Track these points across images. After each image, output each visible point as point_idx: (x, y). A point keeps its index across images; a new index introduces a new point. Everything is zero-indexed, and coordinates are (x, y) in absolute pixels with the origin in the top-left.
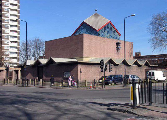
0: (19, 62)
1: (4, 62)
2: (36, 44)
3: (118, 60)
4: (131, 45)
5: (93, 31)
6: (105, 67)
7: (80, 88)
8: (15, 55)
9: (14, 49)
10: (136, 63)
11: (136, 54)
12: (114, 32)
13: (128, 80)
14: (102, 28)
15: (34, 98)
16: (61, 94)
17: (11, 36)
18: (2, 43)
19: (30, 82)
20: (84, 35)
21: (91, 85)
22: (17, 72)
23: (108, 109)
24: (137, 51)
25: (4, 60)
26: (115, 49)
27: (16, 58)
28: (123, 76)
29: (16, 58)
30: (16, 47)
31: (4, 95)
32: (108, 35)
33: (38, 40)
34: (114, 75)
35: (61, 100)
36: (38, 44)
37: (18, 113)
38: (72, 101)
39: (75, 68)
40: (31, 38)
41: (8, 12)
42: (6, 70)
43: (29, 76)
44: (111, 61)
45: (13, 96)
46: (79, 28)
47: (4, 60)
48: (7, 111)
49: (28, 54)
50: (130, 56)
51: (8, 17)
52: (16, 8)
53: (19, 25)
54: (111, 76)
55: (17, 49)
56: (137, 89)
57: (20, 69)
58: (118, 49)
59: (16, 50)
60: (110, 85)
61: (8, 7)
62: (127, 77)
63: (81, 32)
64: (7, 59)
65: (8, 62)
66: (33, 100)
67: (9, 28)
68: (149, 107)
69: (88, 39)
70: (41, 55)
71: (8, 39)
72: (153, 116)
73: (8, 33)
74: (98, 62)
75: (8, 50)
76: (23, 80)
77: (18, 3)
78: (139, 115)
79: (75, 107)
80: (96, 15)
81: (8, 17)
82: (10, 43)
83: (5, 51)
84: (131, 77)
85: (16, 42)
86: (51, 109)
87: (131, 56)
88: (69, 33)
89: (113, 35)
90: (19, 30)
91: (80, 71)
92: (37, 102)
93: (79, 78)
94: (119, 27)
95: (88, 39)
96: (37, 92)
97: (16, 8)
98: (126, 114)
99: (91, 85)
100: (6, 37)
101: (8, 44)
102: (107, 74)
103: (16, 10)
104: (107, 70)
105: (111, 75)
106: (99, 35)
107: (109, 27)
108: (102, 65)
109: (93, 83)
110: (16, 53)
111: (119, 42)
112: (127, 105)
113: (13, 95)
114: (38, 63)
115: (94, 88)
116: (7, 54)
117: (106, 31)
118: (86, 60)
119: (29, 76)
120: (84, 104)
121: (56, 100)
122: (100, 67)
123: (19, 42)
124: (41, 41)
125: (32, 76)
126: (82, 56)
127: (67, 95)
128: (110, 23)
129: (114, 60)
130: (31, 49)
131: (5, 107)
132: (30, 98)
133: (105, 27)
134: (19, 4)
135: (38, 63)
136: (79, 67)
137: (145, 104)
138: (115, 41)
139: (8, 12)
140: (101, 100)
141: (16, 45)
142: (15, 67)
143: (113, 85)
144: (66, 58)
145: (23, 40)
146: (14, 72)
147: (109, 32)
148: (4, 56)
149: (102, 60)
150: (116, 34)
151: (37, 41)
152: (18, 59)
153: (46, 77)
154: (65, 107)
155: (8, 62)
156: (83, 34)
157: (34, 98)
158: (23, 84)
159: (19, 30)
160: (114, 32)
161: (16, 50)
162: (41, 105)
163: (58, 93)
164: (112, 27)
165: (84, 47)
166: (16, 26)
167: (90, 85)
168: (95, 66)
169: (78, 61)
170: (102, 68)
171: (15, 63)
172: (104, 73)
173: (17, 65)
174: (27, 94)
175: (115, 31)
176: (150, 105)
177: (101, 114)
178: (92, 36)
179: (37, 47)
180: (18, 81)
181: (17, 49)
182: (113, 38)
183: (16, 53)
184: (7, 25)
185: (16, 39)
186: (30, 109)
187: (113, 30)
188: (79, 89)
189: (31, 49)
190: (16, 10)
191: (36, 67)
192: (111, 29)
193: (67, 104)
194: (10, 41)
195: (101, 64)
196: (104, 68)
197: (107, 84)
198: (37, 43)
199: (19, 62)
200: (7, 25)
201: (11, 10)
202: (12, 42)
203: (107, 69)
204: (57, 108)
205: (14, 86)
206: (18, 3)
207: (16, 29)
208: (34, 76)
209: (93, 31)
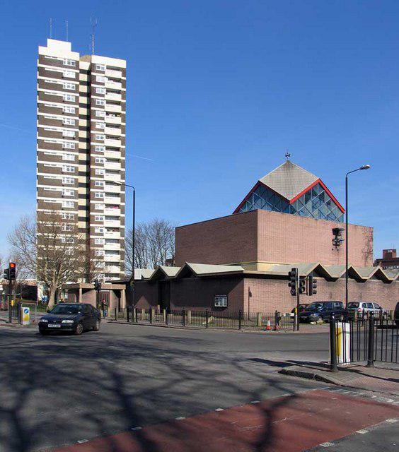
0: (122, 272)
1: (95, 271)
2: (158, 234)
3: (335, 268)
4: (368, 234)
5: (280, 203)
6: (301, 285)
7: (244, 330)
8: (116, 258)
9: (114, 244)
10: (379, 275)
11: (386, 253)
12: (328, 204)
13: (356, 313)
14: (301, 195)
15: (140, 348)
16: (199, 342)
17: (107, 217)
18: (91, 232)
19: (144, 314)
20: (260, 212)
21: (269, 324)
22: (117, 293)
23: (280, 372)
24: (389, 247)
25: (94, 269)
26: (331, 244)
27: (116, 264)
28: (344, 305)
29: (116, 264)
30: (117, 241)
31: (86, 341)
32: (316, 212)
33: (162, 225)
34: (324, 303)
35: (194, 352)
36: (162, 234)
37: (102, 374)
38: (213, 356)
39: (238, 286)
40: (146, 218)
41: (103, 165)
42: (95, 289)
43: (142, 301)
44: (319, 271)
45: (102, 342)
46: (249, 197)
47: (94, 269)
48: (82, 370)
49: (142, 254)
50: (366, 258)
51: (102, 177)
52: (117, 155)
53: (123, 192)
54: (317, 304)
55: (119, 245)
56: (348, 333)
57: (123, 287)
58: (337, 243)
59: (116, 247)
60: (312, 323)
61: (102, 153)
62: (355, 307)
63: (254, 205)
64: (99, 267)
65: (102, 272)
66: (137, 351)
67: (103, 200)
68: (366, 371)
69: (269, 223)
70: (169, 257)
71: (102, 223)
72: (361, 386)
73: (102, 211)
74: (285, 271)
75: (102, 246)
76: (128, 310)
77: (122, 145)
78: (337, 385)
79: (214, 367)
80: (288, 166)
81: (102, 177)
82: (105, 230)
83: (97, 248)
84: (364, 306)
85: (118, 228)
86: (166, 368)
87: (369, 260)
88: (226, 209)
89: (326, 210)
90: (123, 204)
91: (247, 292)
92: (143, 356)
93: (246, 310)
94: (337, 192)
95: (269, 223)
96: (150, 337)
97: (117, 155)
98: (314, 381)
99: (269, 324)
100: (97, 218)
101: (102, 235)
102: (306, 300)
103: (118, 160)
104: (305, 292)
105: (316, 303)
106: (293, 211)
107: (317, 194)
108: (294, 281)
109: (274, 320)
110: (117, 252)
111: (339, 226)
112: (321, 365)
113: (102, 340)
114: (160, 274)
115: (274, 330)
116: (99, 255)
117: (310, 203)
118: (263, 267)
119: (142, 301)
120: (235, 362)
121: (184, 353)
122: (290, 285)
123: (123, 229)
124: (168, 226)
125: (146, 302)
126: (254, 260)
127: (208, 343)
128: (320, 184)
129: (326, 267)
130: (148, 244)
131: (81, 362)
132: (134, 347)
133: (308, 194)
134: (124, 147)
135: (160, 274)
136: (248, 284)
137: (358, 363)
138: (331, 225)
139: (103, 165)
140: (277, 354)
141: (116, 235)
142: (114, 283)
143: (320, 324)
144: (220, 264)
145: (127, 227)
146: (112, 295)
147: (318, 205)
148: (94, 260)
149: (294, 270)
150: (334, 208)
151: (159, 227)
152: (123, 267)
153: (177, 305)
154: (194, 367)
155: (102, 272)
156: (256, 211)
157: (140, 348)
158: (128, 318)
159: (123, 204)
160: (328, 204)
161: (116, 247)
162: (151, 362)
163: (192, 340)
164: (325, 194)
165: (260, 239)
166: (117, 195)
167: (266, 323)
168: (283, 281)
169: (245, 272)
170: (293, 287)
171: (117, 275)
172: (298, 298)
173: (119, 279)
174: (129, 339)
175: (332, 202)
176: (369, 365)
177: (258, 381)
178: (277, 215)
179: (159, 241)
180: (119, 311)
181: (119, 245)
182: (327, 218)
183: (117, 252)
184: (100, 194)
185: (117, 224)
186: (124, 367)
187: (327, 199)
188: (242, 333)
189: (148, 244)
190: (118, 160)
191: (157, 285)
192: (322, 197)
193: (201, 361)
194: (106, 228)
195: (291, 277)
196: (298, 286)
197: (308, 321)
198: (158, 231)
199: (122, 272)
200: (100, 194)
201: (109, 160)
202: (109, 229)
203: (304, 288)
204: (177, 368)
205: (111, 321)
206: (122, 145)
207: (117, 201)
208: (153, 304)
209: (280, 203)
